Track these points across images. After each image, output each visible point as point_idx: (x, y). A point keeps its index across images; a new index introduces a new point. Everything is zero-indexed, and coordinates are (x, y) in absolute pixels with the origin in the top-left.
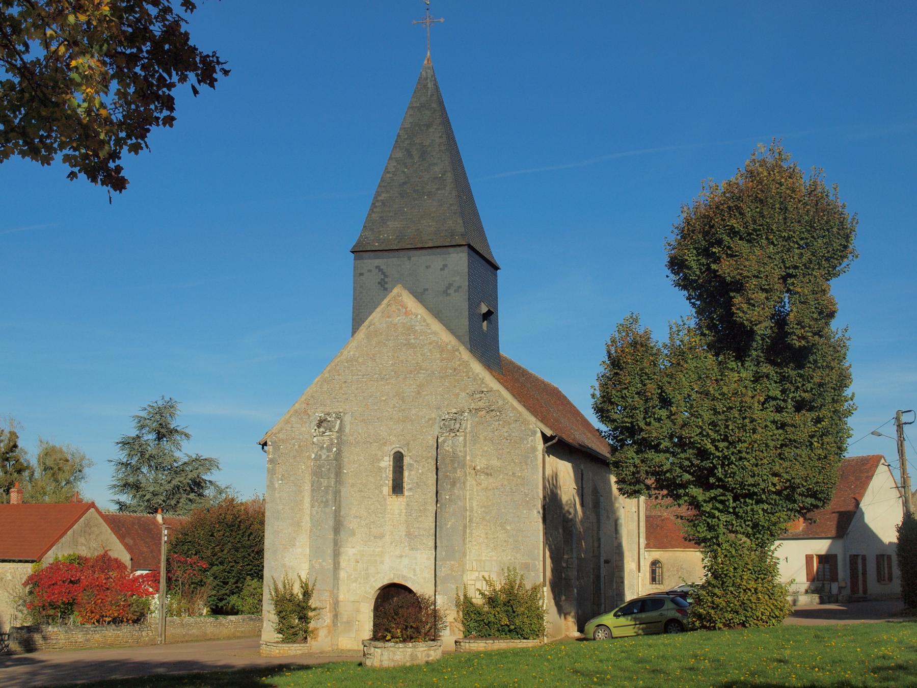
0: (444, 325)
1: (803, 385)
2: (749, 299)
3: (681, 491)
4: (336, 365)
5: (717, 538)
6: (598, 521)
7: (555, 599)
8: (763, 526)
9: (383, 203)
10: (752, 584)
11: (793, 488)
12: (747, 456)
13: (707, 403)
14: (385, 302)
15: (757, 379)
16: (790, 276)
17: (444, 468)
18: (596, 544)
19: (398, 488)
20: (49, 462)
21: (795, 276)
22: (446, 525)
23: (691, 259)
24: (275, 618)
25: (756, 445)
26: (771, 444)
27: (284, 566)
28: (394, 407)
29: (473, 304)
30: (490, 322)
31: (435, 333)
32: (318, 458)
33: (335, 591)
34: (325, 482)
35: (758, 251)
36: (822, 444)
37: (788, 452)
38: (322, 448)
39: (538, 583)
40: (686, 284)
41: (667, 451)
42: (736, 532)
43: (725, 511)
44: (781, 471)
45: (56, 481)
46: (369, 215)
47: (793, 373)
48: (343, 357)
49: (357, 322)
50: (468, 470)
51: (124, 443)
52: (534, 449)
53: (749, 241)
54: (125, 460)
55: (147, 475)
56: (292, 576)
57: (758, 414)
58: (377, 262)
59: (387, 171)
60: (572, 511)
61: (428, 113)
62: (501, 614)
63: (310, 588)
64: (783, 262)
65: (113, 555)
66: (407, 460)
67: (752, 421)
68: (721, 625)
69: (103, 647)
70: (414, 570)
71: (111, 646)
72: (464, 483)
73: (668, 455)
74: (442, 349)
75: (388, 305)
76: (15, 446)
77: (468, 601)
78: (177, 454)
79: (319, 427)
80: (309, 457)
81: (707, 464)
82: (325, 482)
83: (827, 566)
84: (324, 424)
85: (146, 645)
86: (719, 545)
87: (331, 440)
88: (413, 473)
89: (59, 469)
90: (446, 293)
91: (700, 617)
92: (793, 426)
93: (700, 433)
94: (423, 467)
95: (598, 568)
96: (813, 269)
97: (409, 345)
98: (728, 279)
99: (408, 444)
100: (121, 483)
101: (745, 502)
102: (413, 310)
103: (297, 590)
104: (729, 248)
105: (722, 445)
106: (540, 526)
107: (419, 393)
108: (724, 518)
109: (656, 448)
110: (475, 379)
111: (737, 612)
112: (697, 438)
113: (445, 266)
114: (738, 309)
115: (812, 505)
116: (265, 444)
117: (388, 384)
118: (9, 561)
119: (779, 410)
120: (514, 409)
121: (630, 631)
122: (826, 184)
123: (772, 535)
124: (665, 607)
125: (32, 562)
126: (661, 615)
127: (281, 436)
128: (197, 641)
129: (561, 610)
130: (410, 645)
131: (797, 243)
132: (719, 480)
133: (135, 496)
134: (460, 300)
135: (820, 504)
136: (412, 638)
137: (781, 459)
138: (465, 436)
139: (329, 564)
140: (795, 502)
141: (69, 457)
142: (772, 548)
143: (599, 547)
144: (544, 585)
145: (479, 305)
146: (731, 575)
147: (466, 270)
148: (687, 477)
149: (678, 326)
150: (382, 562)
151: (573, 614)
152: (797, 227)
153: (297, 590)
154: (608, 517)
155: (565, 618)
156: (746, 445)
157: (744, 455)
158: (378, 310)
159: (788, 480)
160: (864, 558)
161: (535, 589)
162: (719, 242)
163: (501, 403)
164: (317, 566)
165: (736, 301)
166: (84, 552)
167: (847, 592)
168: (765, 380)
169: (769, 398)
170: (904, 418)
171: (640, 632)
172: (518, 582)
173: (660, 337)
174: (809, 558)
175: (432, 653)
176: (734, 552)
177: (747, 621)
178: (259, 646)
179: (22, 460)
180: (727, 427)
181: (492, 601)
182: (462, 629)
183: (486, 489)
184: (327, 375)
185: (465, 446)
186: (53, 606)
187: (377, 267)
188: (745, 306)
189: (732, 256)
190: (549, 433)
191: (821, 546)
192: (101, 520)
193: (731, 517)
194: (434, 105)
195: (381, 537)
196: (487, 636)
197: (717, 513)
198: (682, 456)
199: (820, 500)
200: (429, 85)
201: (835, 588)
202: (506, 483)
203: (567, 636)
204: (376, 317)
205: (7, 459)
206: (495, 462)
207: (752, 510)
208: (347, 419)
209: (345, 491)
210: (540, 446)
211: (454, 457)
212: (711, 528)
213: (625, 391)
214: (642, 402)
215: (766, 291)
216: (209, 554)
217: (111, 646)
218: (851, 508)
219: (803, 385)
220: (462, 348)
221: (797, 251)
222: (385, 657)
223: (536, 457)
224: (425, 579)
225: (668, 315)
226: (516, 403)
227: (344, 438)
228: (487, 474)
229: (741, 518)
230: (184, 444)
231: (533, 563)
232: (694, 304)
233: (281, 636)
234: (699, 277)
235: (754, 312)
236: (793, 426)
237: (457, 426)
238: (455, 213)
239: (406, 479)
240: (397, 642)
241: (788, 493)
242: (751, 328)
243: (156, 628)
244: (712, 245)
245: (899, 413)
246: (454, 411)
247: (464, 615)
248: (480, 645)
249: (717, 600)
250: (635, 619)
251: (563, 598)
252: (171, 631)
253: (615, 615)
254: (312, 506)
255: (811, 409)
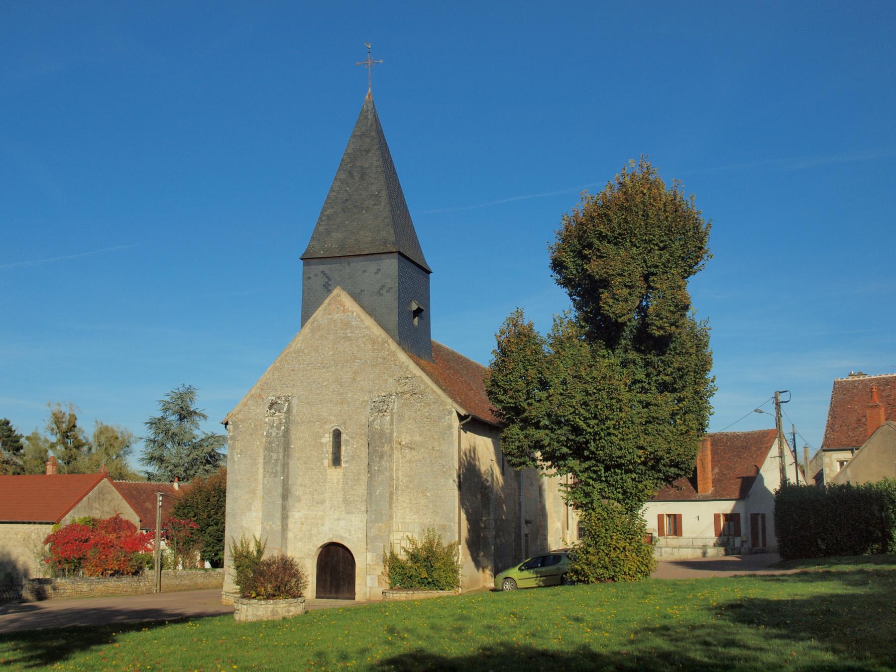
0: (375, 320)
1: (665, 369)
2: (614, 295)
3: (561, 462)
4: (286, 356)
5: (592, 503)
6: (519, 488)
7: (472, 555)
8: (631, 493)
9: (328, 217)
10: (622, 544)
11: (658, 460)
12: (615, 432)
13: (580, 386)
14: (327, 301)
15: (624, 364)
16: (653, 274)
17: (377, 445)
18: (517, 508)
19: (336, 460)
20: (103, 439)
21: (655, 274)
22: (375, 492)
23: (569, 261)
24: (233, 572)
25: (622, 422)
26: (637, 421)
27: (242, 527)
28: (334, 391)
29: (403, 301)
30: (421, 318)
31: (368, 328)
32: (269, 435)
33: (284, 549)
34: (274, 456)
35: (622, 253)
36: (685, 421)
37: (650, 427)
38: (272, 426)
39: (453, 542)
40: (566, 282)
41: (546, 427)
42: (608, 498)
43: (598, 479)
44: (645, 444)
45: (108, 455)
46: (316, 227)
47: (655, 359)
48: (292, 349)
49: (306, 316)
50: (395, 445)
51: (152, 423)
52: (450, 427)
53: (615, 244)
54: (152, 437)
55: (171, 451)
56: (249, 536)
57: (626, 396)
58: (322, 268)
59: (332, 190)
60: (489, 479)
61: (368, 140)
62: (421, 569)
63: (262, 546)
64: (645, 261)
65: (124, 517)
66: (344, 437)
67: (619, 401)
68: (593, 580)
69: (105, 596)
70: (350, 531)
71: (113, 594)
72: (391, 456)
73: (547, 431)
74: (373, 341)
75: (329, 304)
76: (74, 426)
77: (393, 557)
78: (196, 432)
79: (270, 409)
80: (262, 434)
81: (581, 439)
82: (274, 456)
83: (732, 523)
84: (275, 406)
85: (143, 594)
86: (593, 510)
87: (280, 419)
88: (349, 447)
89: (111, 445)
90: (379, 293)
91: (576, 572)
92: (655, 405)
93: (574, 412)
94: (358, 442)
95: (519, 527)
96: (671, 268)
97: (346, 338)
98: (597, 277)
99: (345, 423)
100: (149, 456)
101: (615, 472)
102: (350, 308)
103: (252, 548)
104: (598, 250)
105: (592, 422)
106: (456, 493)
107: (354, 379)
108: (598, 486)
109: (537, 426)
110: (401, 367)
111: (607, 568)
112: (570, 416)
113: (379, 270)
114: (604, 303)
115: (675, 474)
116: (227, 424)
117: (328, 371)
118: (29, 523)
119: (644, 390)
120: (434, 392)
121: (533, 583)
122: (684, 194)
123: (640, 500)
124: (562, 562)
125: (53, 523)
126: (558, 569)
127: (240, 416)
128: (188, 590)
129: (478, 564)
130: (272, 602)
131: (657, 245)
132: (592, 453)
133: (160, 467)
134: (391, 299)
135: (682, 473)
136: (274, 596)
137: (646, 434)
138: (392, 416)
139: (277, 526)
140: (660, 471)
141: (119, 435)
142: (640, 512)
143: (520, 510)
144: (460, 543)
145: (409, 303)
146: (603, 535)
147: (396, 274)
148: (565, 450)
149: (561, 319)
150: (323, 525)
151: (490, 567)
152: (657, 231)
153: (252, 548)
154: (532, 484)
155: (483, 571)
156: (613, 422)
157: (612, 431)
158: (320, 308)
159: (651, 453)
160: (763, 516)
161: (451, 547)
162: (590, 246)
163: (422, 387)
164: (268, 528)
165: (603, 296)
166: (97, 514)
167: (748, 545)
168: (632, 365)
169: (635, 382)
170: (782, 398)
171: (541, 583)
172: (436, 541)
173: (543, 328)
174: (717, 517)
175: (292, 609)
176: (606, 516)
177: (615, 576)
178: (221, 596)
179: (81, 437)
180: (597, 406)
181: (414, 557)
182: (388, 581)
183: (410, 461)
184: (278, 364)
185: (392, 424)
186: (67, 561)
187: (323, 272)
188: (611, 301)
189: (601, 257)
190: (463, 412)
191: (727, 507)
192: (114, 489)
193: (604, 485)
194: (373, 134)
195: (323, 502)
196: (411, 587)
197: (591, 482)
198: (559, 432)
199: (681, 469)
200: (370, 117)
201: (738, 542)
202: (426, 456)
203: (484, 587)
204: (319, 314)
205: (67, 437)
206: (417, 438)
207: (622, 479)
208: (295, 402)
209: (292, 463)
210: (456, 423)
211: (382, 434)
212: (587, 495)
213: (510, 376)
214: (524, 385)
215: (630, 287)
216: (205, 516)
217: (113, 594)
218: (752, 473)
219: (665, 369)
220: (390, 340)
221: (657, 252)
222: (250, 613)
223: (452, 433)
224: (358, 538)
225: (550, 310)
226: (435, 388)
227: (291, 418)
228: (411, 448)
229: (613, 486)
230: (202, 423)
231: (451, 524)
232: (574, 300)
233: (239, 587)
234: (575, 275)
235: (619, 305)
236: (655, 405)
237: (385, 407)
238: (388, 225)
239: (343, 453)
240: (260, 600)
241: (653, 463)
242: (616, 321)
243: (152, 580)
244: (584, 247)
245: (777, 393)
246: (383, 394)
247: (390, 569)
248: (402, 596)
249: (591, 558)
250: (537, 573)
251: (482, 554)
252: (165, 581)
253: (520, 569)
254: (264, 477)
255: (674, 390)
